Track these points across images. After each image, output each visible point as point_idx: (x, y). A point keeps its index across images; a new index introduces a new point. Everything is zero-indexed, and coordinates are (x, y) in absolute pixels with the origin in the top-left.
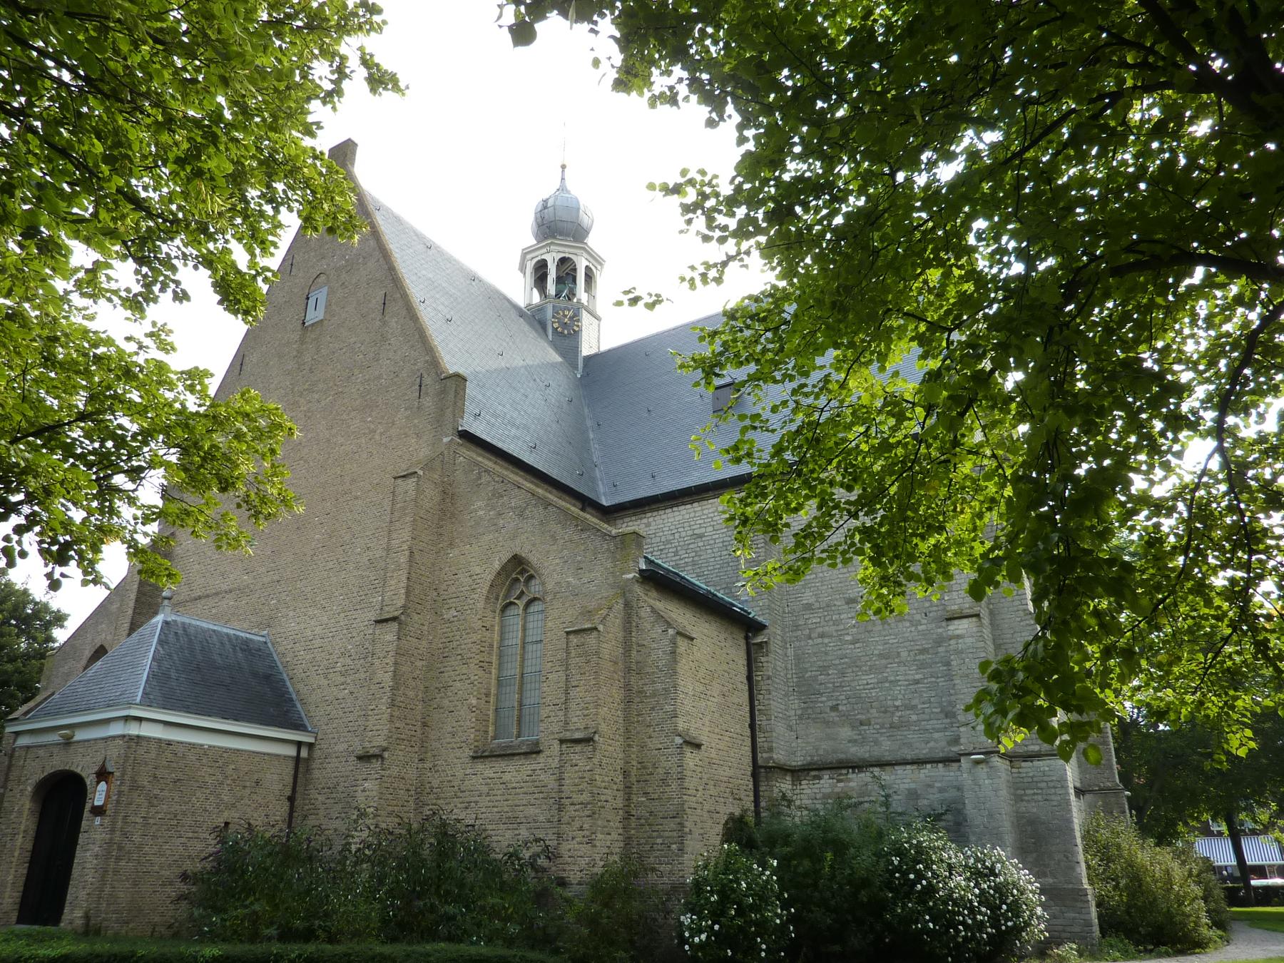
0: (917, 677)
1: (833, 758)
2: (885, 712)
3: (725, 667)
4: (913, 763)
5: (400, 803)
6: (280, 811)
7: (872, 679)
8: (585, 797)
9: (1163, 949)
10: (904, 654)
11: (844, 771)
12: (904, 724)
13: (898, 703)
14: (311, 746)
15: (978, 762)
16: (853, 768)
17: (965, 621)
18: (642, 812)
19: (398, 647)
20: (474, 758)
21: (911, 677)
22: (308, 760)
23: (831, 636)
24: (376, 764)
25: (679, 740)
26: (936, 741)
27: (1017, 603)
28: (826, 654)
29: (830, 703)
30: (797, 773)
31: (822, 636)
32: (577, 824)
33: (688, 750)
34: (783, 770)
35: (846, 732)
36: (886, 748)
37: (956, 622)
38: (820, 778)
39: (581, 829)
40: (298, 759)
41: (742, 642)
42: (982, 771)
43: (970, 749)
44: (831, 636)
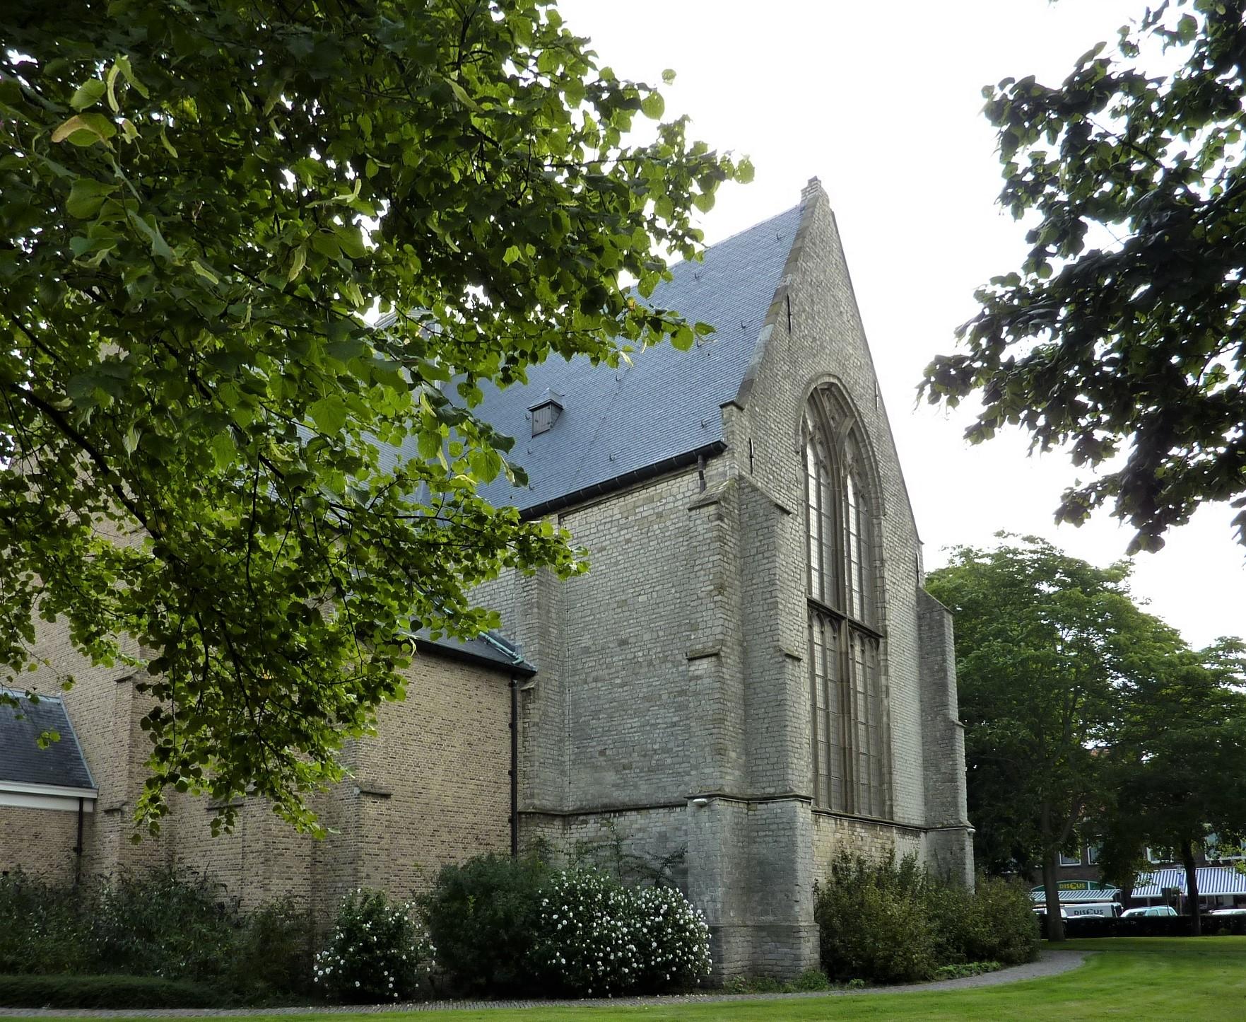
0: (675, 719)
1: (599, 802)
2: (645, 756)
3: (476, 716)
4: (664, 807)
5: (147, 853)
6: (63, 859)
7: (636, 722)
8: (260, 846)
9: (854, 982)
10: (665, 697)
11: (607, 815)
12: (660, 768)
13: (656, 747)
14: (94, 801)
15: (701, 806)
16: (615, 812)
17: (705, 661)
18: (329, 858)
19: (134, 706)
20: (209, 810)
21: (669, 720)
22: (93, 815)
23: (603, 680)
24: (118, 817)
25: (357, 791)
26: (686, 784)
27: (769, 639)
28: (599, 698)
29: (599, 748)
30: (568, 818)
31: (596, 680)
32: (254, 870)
33: (368, 802)
34: (548, 815)
35: (610, 777)
36: (643, 792)
37: (697, 662)
38: (586, 822)
39: (257, 875)
40: (81, 814)
41: (506, 691)
42: (705, 813)
43: (697, 793)
44: (603, 680)
